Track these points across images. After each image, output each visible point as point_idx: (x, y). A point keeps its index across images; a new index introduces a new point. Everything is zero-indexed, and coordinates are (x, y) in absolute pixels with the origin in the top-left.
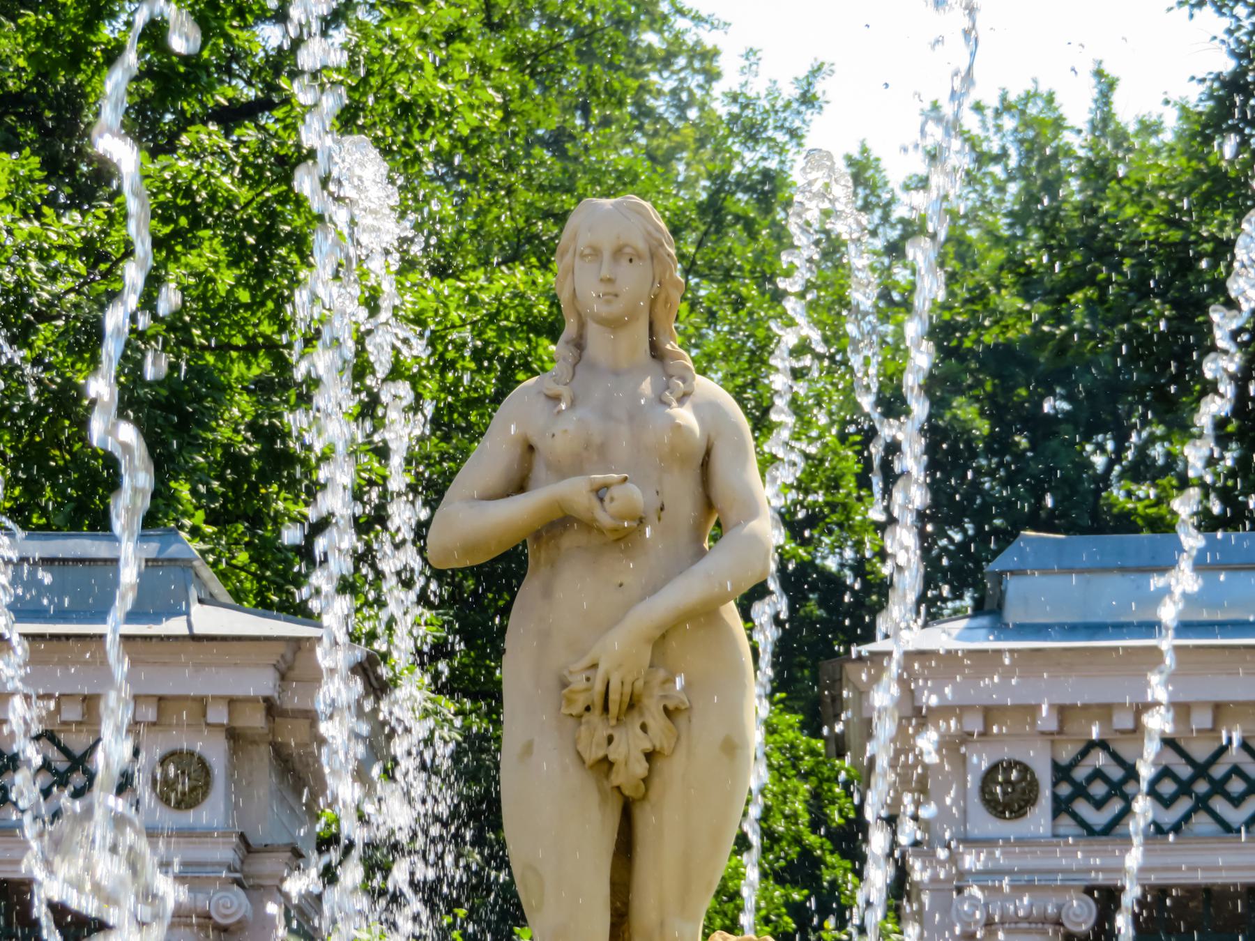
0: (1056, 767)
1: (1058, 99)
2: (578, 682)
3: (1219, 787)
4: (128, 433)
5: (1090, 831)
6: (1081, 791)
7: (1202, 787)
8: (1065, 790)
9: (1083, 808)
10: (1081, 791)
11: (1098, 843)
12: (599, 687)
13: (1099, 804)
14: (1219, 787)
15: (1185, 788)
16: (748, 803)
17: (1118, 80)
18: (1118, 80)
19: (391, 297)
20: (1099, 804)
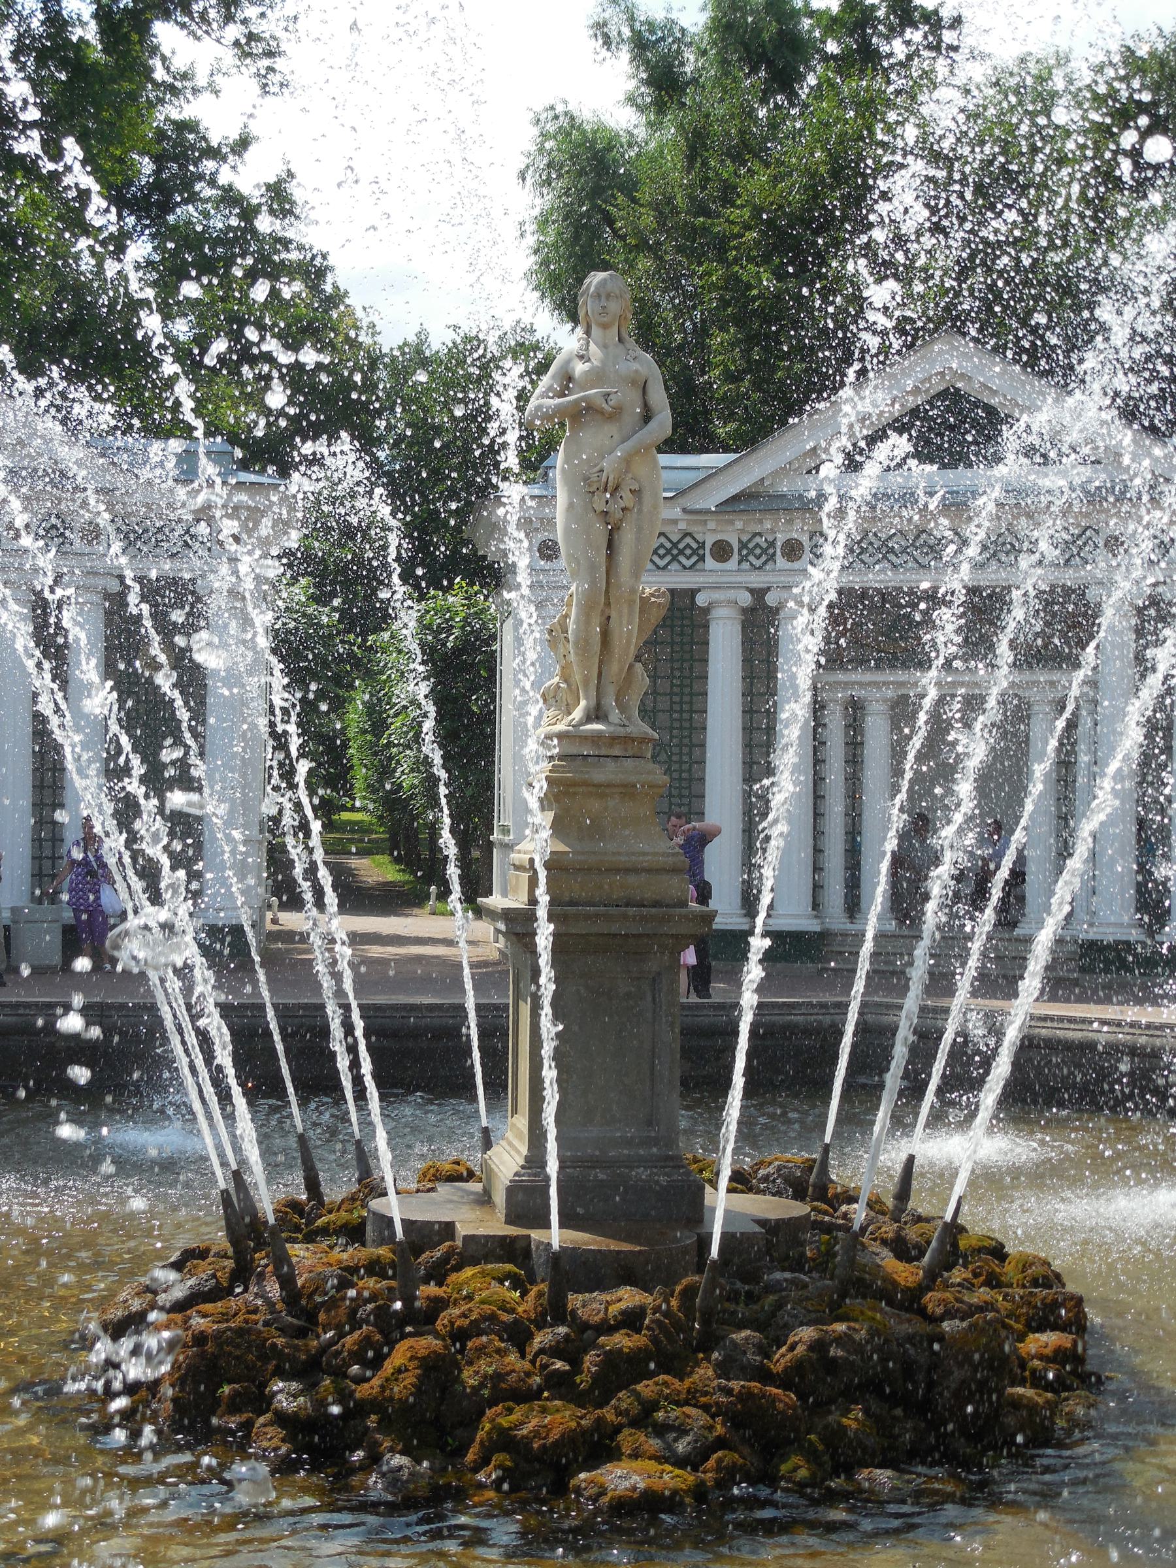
0: (740, 541)
1: (258, 90)
2: (594, 478)
3: (681, 552)
4: (145, 608)
5: (658, 567)
6: (694, 552)
7: (675, 552)
8: (701, 552)
9: (682, 559)
10: (751, 551)
11: (687, 573)
12: (604, 479)
13: (688, 558)
14: (681, 552)
15: (668, 551)
16: (96, 574)
17: (257, 139)
18: (257, 139)
19: (156, 666)
20: (688, 558)
